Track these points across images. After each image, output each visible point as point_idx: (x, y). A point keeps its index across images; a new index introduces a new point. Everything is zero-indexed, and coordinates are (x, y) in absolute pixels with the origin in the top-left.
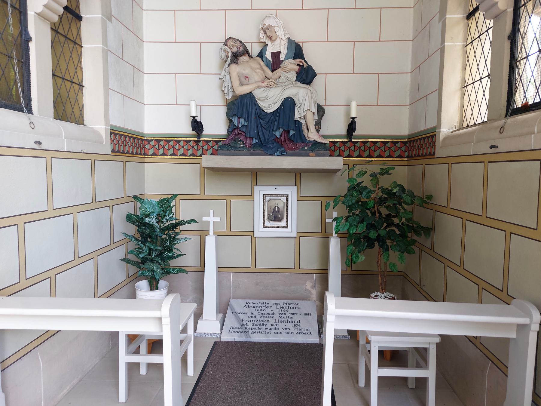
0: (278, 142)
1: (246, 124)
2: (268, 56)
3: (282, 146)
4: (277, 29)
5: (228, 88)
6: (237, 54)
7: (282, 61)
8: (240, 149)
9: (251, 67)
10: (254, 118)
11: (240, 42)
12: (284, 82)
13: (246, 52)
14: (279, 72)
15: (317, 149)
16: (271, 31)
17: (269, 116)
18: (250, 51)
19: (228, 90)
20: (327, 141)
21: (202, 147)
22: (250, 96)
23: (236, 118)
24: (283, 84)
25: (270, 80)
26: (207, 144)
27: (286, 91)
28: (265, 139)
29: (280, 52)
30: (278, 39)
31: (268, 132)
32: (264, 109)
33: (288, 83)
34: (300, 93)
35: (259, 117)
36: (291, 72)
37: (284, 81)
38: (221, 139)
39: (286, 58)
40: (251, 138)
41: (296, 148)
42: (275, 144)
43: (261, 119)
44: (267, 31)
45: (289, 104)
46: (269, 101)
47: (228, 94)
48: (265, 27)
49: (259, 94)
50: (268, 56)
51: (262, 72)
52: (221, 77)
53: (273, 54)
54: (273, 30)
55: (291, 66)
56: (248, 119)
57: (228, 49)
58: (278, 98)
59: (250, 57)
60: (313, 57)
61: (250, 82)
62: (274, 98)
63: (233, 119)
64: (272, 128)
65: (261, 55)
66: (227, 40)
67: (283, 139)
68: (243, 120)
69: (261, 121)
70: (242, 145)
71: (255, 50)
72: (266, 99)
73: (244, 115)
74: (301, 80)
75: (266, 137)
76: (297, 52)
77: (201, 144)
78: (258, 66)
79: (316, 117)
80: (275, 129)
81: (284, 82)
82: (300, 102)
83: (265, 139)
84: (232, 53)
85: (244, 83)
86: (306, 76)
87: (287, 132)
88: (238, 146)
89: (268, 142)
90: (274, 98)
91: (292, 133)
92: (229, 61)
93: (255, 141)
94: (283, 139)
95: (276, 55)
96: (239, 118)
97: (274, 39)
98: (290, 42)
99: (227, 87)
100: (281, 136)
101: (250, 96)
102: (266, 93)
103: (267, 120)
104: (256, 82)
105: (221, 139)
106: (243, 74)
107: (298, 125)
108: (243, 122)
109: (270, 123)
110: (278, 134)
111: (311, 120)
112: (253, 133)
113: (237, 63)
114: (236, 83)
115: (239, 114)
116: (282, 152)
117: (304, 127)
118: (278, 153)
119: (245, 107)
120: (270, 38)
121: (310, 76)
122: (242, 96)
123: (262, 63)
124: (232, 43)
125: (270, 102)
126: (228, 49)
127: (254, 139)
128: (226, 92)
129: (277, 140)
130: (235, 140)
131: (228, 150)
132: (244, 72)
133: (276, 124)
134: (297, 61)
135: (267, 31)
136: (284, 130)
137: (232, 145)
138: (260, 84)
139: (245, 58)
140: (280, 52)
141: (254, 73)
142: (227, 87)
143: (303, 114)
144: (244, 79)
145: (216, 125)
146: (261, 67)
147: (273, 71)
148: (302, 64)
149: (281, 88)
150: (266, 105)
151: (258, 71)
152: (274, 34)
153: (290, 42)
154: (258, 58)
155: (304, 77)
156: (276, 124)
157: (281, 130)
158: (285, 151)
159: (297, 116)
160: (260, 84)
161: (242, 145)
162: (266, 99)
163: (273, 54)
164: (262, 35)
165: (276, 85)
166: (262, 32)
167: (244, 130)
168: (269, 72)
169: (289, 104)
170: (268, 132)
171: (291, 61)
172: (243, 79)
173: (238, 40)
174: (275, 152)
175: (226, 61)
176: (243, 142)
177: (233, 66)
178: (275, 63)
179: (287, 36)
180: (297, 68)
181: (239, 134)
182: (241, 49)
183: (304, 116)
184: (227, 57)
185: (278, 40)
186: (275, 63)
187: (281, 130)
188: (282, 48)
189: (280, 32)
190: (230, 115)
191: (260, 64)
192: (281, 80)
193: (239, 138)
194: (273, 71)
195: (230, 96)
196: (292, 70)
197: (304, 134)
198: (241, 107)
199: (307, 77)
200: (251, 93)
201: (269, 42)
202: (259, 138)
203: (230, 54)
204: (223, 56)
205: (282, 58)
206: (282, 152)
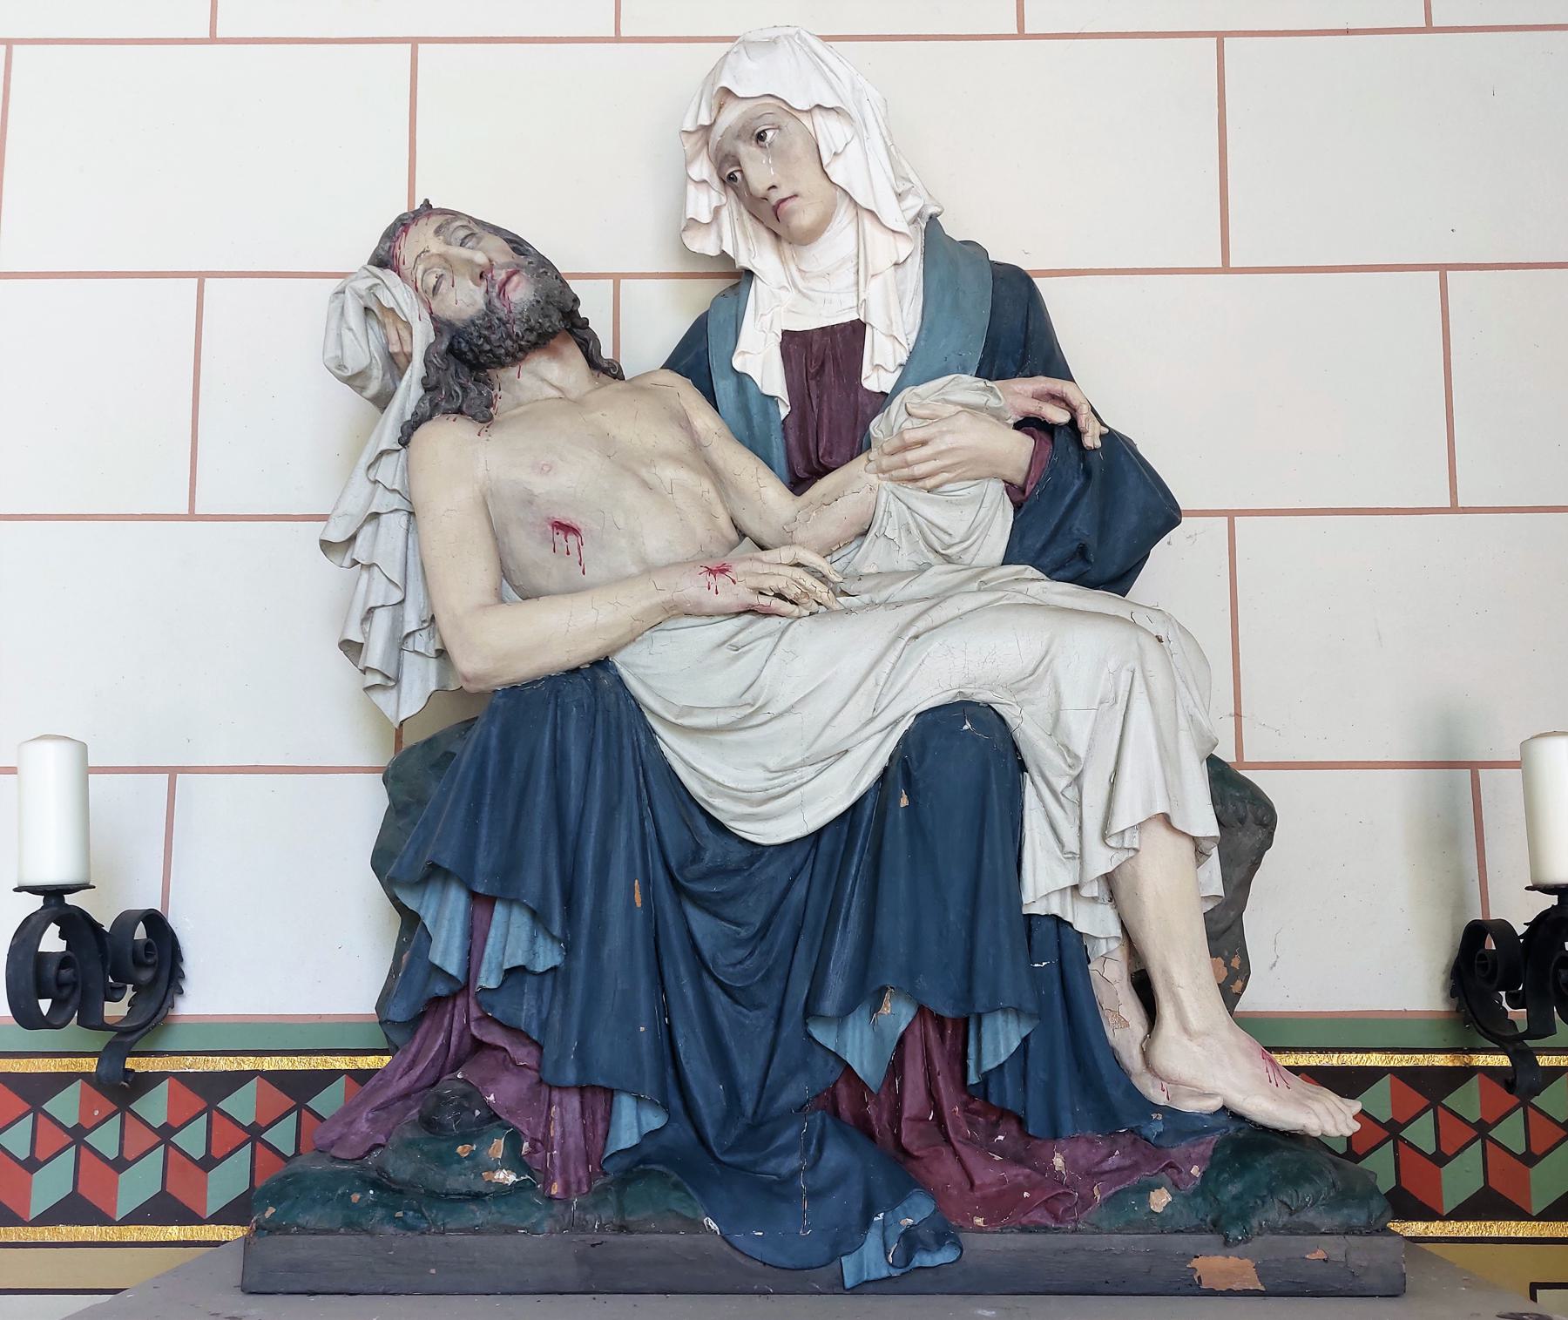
0: (864, 1126)
1: (548, 957)
2: (759, 359)
3: (902, 1170)
4: (830, 131)
5: (397, 622)
6: (488, 339)
7: (882, 400)
8: (478, 1215)
9: (607, 446)
10: (626, 895)
11: (517, 245)
12: (898, 575)
13: (559, 323)
14: (853, 486)
15: (1274, 1214)
16: (780, 155)
17: (776, 871)
18: (600, 325)
19: (400, 642)
20: (1331, 1117)
21: (166, 1133)
22: (592, 695)
23: (456, 899)
24: (898, 591)
25: (786, 554)
26: (211, 1108)
27: (934, 647)
28: (733, 1093)
29: (857, 329)
30: (844, 215)
31: (758, 1021)
32: (722, 808)
33: (938, 577)
34: (1040, 656)
35: (678, 889)
36: (967, 490)
37: (904, 560)
38: (340, 1063)
39: (915, 370)
40: (598, 1097)
41: (1060, 1203)
42: (835, 1156)
43: (699, 901)
44: (750, 165)
45: (960, 771)
46: (779, 736)
47: (392, 681)
48: (732, 115)
49: (673, 678)
50: (759, 359)
51: (706, 485)
52: (337, 534)
53: (793, 344)
54: (800, 148)
55: (965, 432)
56: (567, 909)
57: (397, 293)
58: (858, 709)
59: (604, 369)
60: (1119, 375)
61: (594, 572)
62: (821, 708)
63: (426, 905)
64: (800, 990)
65: (696, 359)
66: (401, 226)
67: (914, 1100)
68: (520, 922)
69: (699, 921)
70: (507, 1177)
71: (645, 323)
72: (747, 715)
73: (531, 884)
74: (1057, 552)
75: (747, 1072)
76: (1006, 327)
77: (155, 1107)
78: (671, 439)
79: (1212, 878)
80: (829, 1005)
81: (898, 575)
82: (1066, 750)
83: (733, 1093)
84: (440, 325)
85: (540, 580)
86: (1091, 514)
87: (954, 1030)
88: (457, 1182)
89: (758, 1131)
90: (821, 708)
91: (1000, 1040)
92: (410, 391)
93: (632, 1123)
94: (914, 1100)
95: (826, 356)
96: (481, 902)
97: (803, 216)
98: (944, 255)
99: (382, 620)
100: (896, 1068)
101: (592, 695)
102: (748, 664)
103: (754, 911)
104: (649, 570)
105: (340, 1063)
106: (529, 500)
107: (1058, 942)
108: (513, 939)
109: (783, 934)
110: (860, 1045)
111: (1173, 896)
112: (622, 1040)
113: (484, 415)
114: (464, 577)
115: (483, 862)
116: (911, 1242)
117: (1109, 977)
118: (871, 1257)
119: (541, 799)
120: (769, 214)
121: (1130, 520)
122: (514, 691)
123: (704, 419)
124: (436, 246)
125: (783, 743)
126: (397, 293)
127: (626, 1106)
128: (375, 655)
129: (850, 1109)
130: (429, 1123)
131: (352, 1226)
132: (541, 485)
133: (844, 950)
134: (1021, 394)
135: (750, 165)
136: (922, 1011)
137: (401, 1168)
138: (693, 587)
139: (552, 374)
140: (857, 329)
141: (631, 494)
142: (382, 620)
143: (1101, 861)
144: (539, 547)
145: (290, 939)
146: (697, 445)
147: (798, 484)
148: (1059, 416)
149: (888, 621)
150: (746, 777)
151: (669, 473)
152: (807, 180)
153: (944, 255)
154: (672, 378)
155: (1082, 526)
156: (844, 950)
157: (897, 1014)
158: (944, 1235)
159: (1044, 882)
160: (693, 587)
161: (507, 1177)
162: (747, 715)
163: (793, 344)
164: (702, 203)
165: (833, 596)
166: (702, 169)
167: (526, 1012)
168: (766, 492)
169: (960, 771)
170: (758, 1021)
171: (966, 388)
172: (530, 548)
173: (496, 231)
174: (844, 1241)
175: (382, 401)
176: (514, 1139)
177: (447, 438)
178: (823, 414)
179: (913, 204)
180: (1018, 450)
181: (479, 1046)
182: (521, 293)
183: (1108, 879)
184: (396, 363)
185: (840, 239)
186: (823, 414)
187: (897, 1014)
188: (874, 291)
189: (858, 166)
190: (401, 864)
191: (685, 424)
192: (871, 557)
193: (472, 1095)
194: (798, 484)
195: (412, 697)
196: (974, 468)
197: (1115, 1036)
198: (518, 787)
199: (1103, 527)
200: (602, 664)
201: (758, 254)
202: (673, 1088)
203: (422, 336)
204: (362, 350)
205: (875, 379)
206: (911, 1242)
